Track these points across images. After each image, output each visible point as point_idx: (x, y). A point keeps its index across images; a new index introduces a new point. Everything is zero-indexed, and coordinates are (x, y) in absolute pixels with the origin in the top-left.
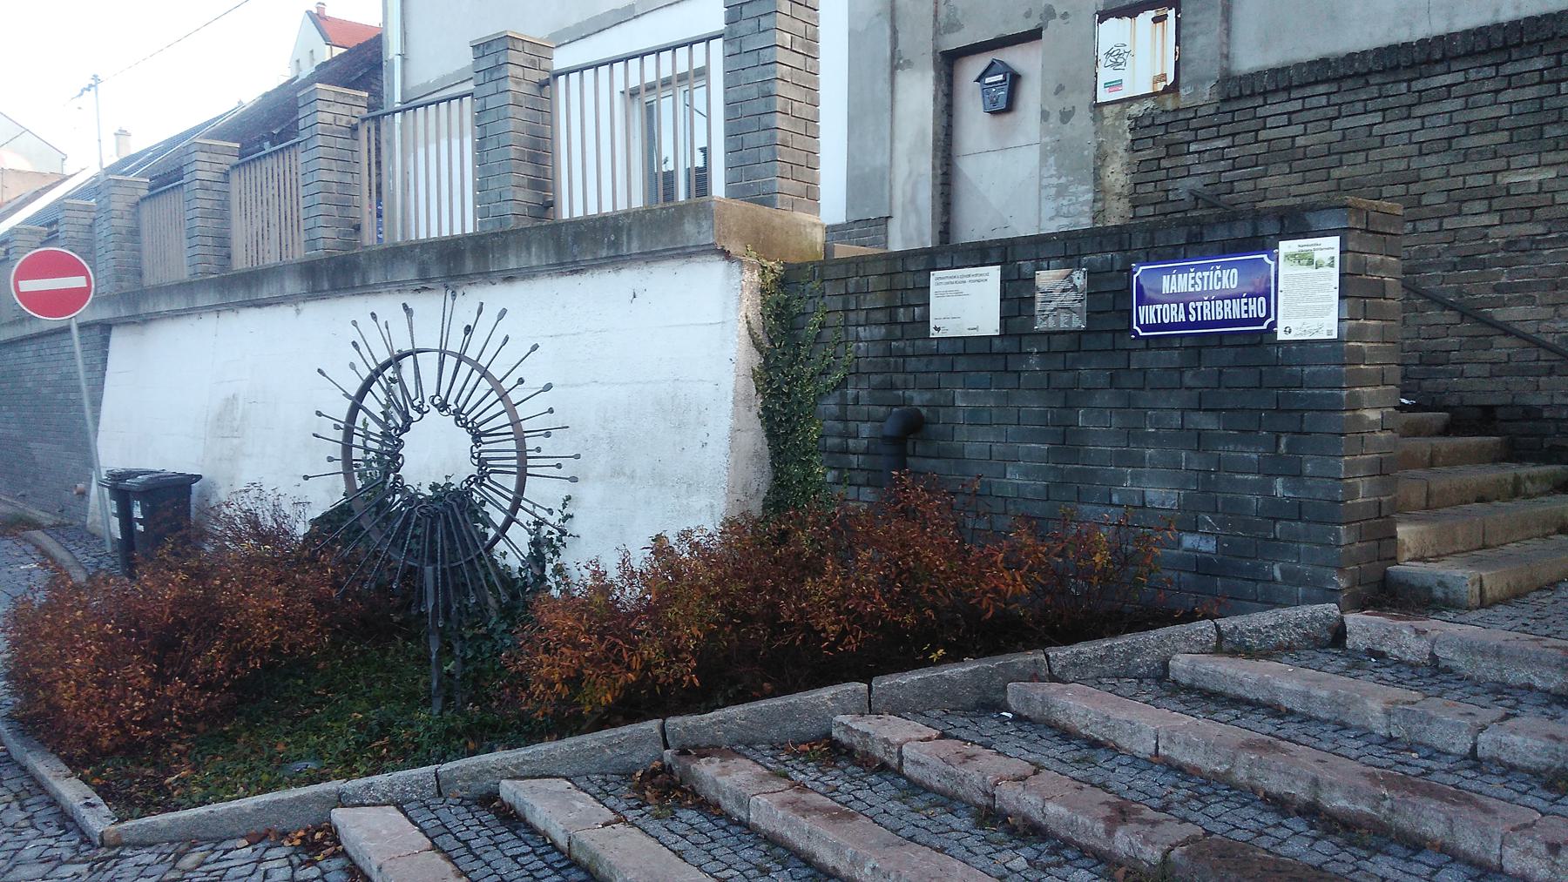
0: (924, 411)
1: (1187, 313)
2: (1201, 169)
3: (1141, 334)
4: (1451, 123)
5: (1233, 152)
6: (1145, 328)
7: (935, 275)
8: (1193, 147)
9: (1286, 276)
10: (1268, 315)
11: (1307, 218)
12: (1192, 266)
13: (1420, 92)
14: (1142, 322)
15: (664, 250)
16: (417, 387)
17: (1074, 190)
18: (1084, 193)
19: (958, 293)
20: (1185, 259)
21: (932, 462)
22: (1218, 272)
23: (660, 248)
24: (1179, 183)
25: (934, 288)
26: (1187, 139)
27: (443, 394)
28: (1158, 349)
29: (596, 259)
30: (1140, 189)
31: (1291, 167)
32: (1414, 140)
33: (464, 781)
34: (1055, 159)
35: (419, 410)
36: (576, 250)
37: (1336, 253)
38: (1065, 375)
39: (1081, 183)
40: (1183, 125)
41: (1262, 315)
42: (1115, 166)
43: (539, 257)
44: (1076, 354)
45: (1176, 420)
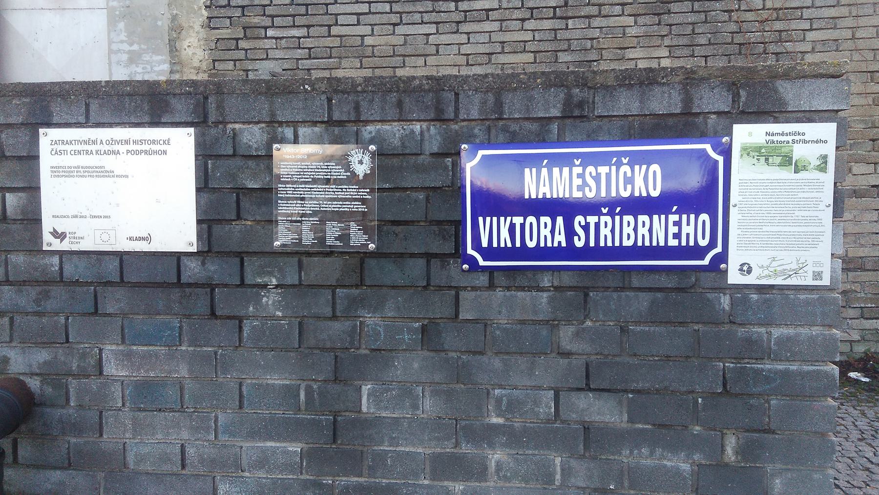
0: (34, 384)
1: (570, 233)
2: (278, 54)
3: (482, 263)
4: (490, 42)
5: (309, 43)
6: (489, 253)
7: (48, 137)
8: (270, 33)
9: (742, 182)
10: (712, 244)
11: (781, 90)
12: (577, 156)
13: (465, 11)
14: (485, 244)
17: (148, 58)
18: (160, 63)
19: (107, 174)
20: (560, 143)
21: (57, 475)
22: (625, 169)
24: (258, 65)
25: (47, 160)
26: (263, 24)
28: (508, 288)
30: (219, 66)
31: (361, 62)
32: (462, 52)
37: (830, 150)
38: (337, 325)
39: (156, 52)
40: (259, 10)
41: (703, 243)
42: (192, 40)
44: (355, 292)
45: (546, 405)
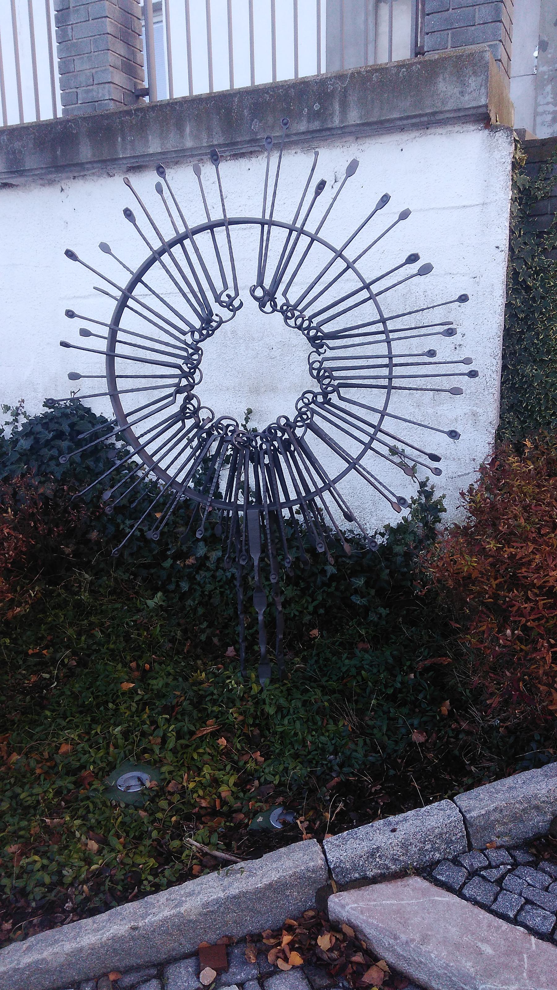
15: (401, 119)
16: (264, 266)
23: (396, 115)
27: (268, 282)
29: (288, 136)
33: (505, 824)
34: (553, 88)
35: (229, 306)
36: (256, 125)
43: (197, 137)
